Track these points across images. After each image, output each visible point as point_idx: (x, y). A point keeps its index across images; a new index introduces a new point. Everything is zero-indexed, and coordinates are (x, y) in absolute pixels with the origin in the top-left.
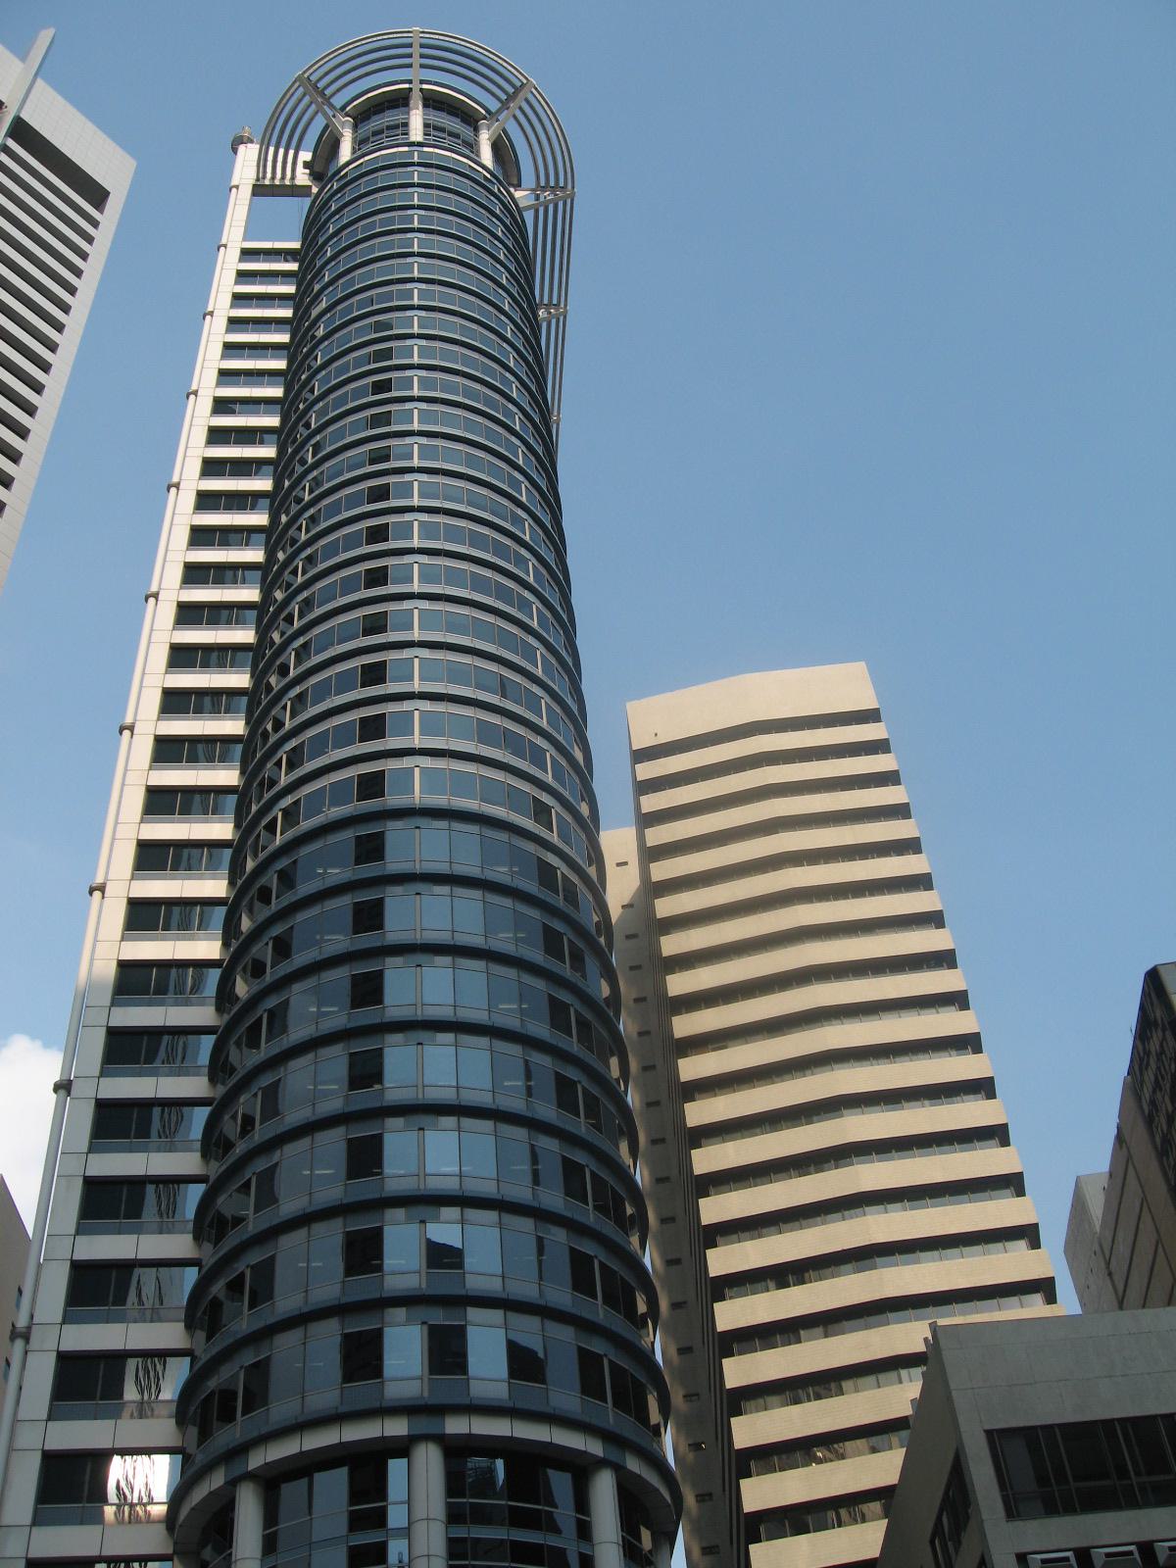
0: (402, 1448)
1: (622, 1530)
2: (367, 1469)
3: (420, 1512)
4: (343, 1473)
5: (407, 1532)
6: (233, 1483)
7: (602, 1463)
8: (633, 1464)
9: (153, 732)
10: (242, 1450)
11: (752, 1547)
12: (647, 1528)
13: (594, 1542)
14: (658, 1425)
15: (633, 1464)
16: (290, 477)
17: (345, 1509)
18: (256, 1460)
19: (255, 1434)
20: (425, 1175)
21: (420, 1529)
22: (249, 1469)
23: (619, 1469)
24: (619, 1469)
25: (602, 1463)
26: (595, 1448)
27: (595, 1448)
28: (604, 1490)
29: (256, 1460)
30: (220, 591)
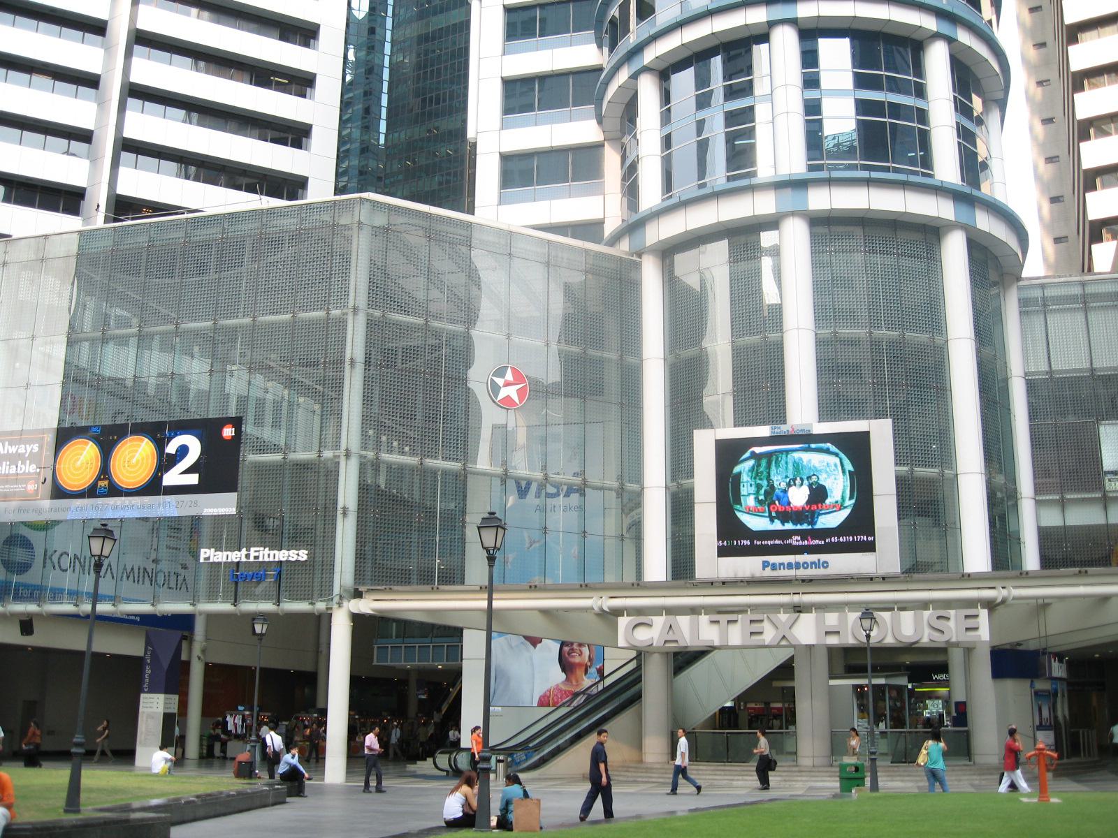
0: (772, 223)
1: (954, 91)
2: (743, 237)
3: (778, 81)
4: (724, 244)
5: (771, 97)
6: (635, 76)
7: (937, 36)
8: (964, 37)
9: (500, 76)
10: (638, 49)
11: (1094, 247)
12: (979, 96)
13: (929, 100)
14: (990, 22)
15: (964, 37)
16: (613, 22)
17: (720, 84)
18: (649, 55)
19: (646, 35)
20: (814, 766)
21: (779, 95)
22: (645, 64)
23: (950, 41)
24: (950, 41)
25: (937, 36)
26: (929, 23)
27: (929, 23)
28: (954, 251)
29: (649, 55)
30: (548, 52)
